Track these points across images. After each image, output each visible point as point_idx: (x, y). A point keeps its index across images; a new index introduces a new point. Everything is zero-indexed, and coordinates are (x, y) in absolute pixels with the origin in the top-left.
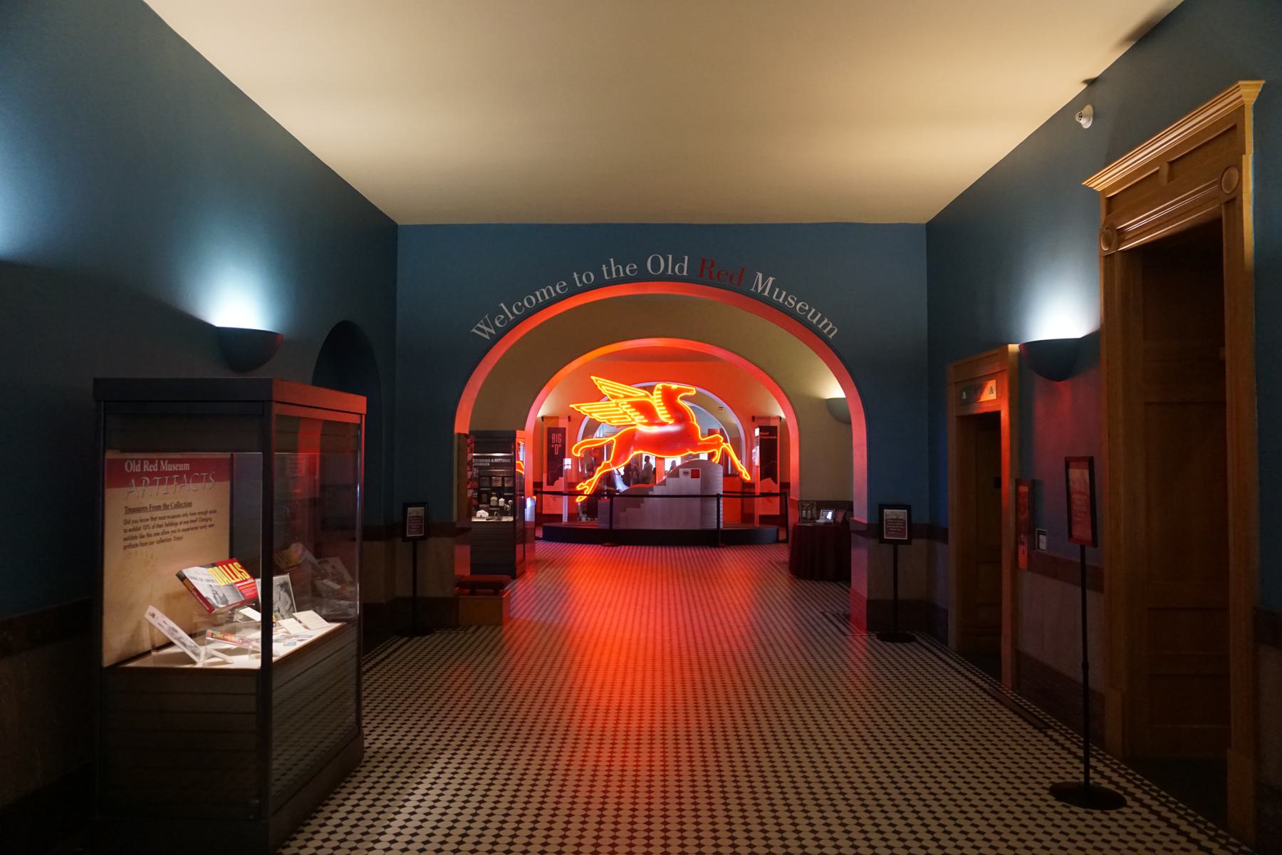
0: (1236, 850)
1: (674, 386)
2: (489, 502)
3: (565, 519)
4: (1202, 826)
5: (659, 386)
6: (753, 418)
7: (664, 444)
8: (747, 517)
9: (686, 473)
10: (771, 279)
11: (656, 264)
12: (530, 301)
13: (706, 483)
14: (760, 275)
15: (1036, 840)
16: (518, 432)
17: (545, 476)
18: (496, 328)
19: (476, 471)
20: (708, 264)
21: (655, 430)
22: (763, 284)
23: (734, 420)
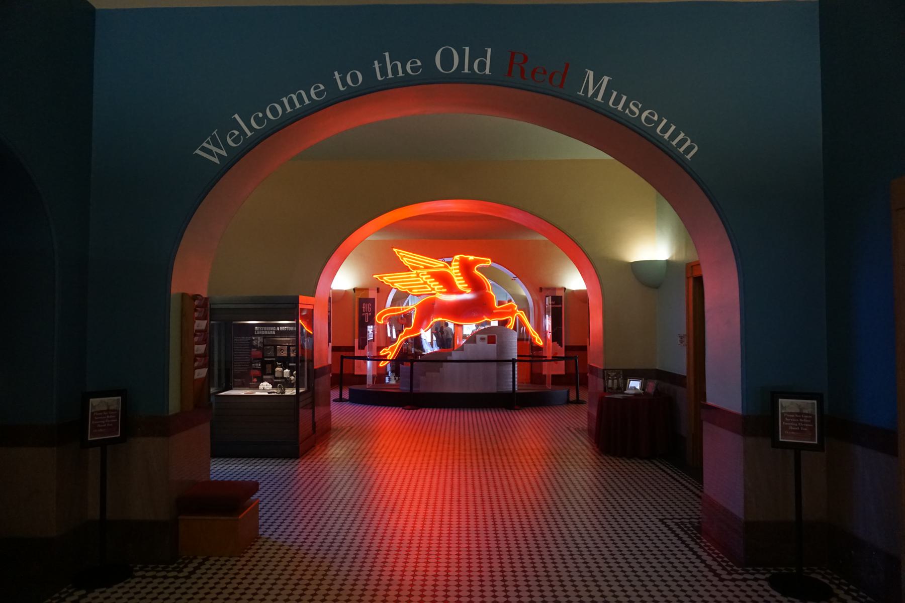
0: (863, 600)
1: (471, 258)
2: (273, 373)
3: (369, 381)
4: (855, 594)
5: (457, 257)
6: (541, 289)
7: (462, 311)
8: (536, 378)
9: (482, 339)
10: (606, 79)
11: (447, 60)
12: (274, 111)
13: (502, 348)
14: (591, 74)
15: (721, 591)
16: (302, 299)
17: (356, 341)
18: (227, 147)
19: (260, 340)
20: (519, 59)
21: (453, 298)
22: (595, 86)
23: (523, 292)
